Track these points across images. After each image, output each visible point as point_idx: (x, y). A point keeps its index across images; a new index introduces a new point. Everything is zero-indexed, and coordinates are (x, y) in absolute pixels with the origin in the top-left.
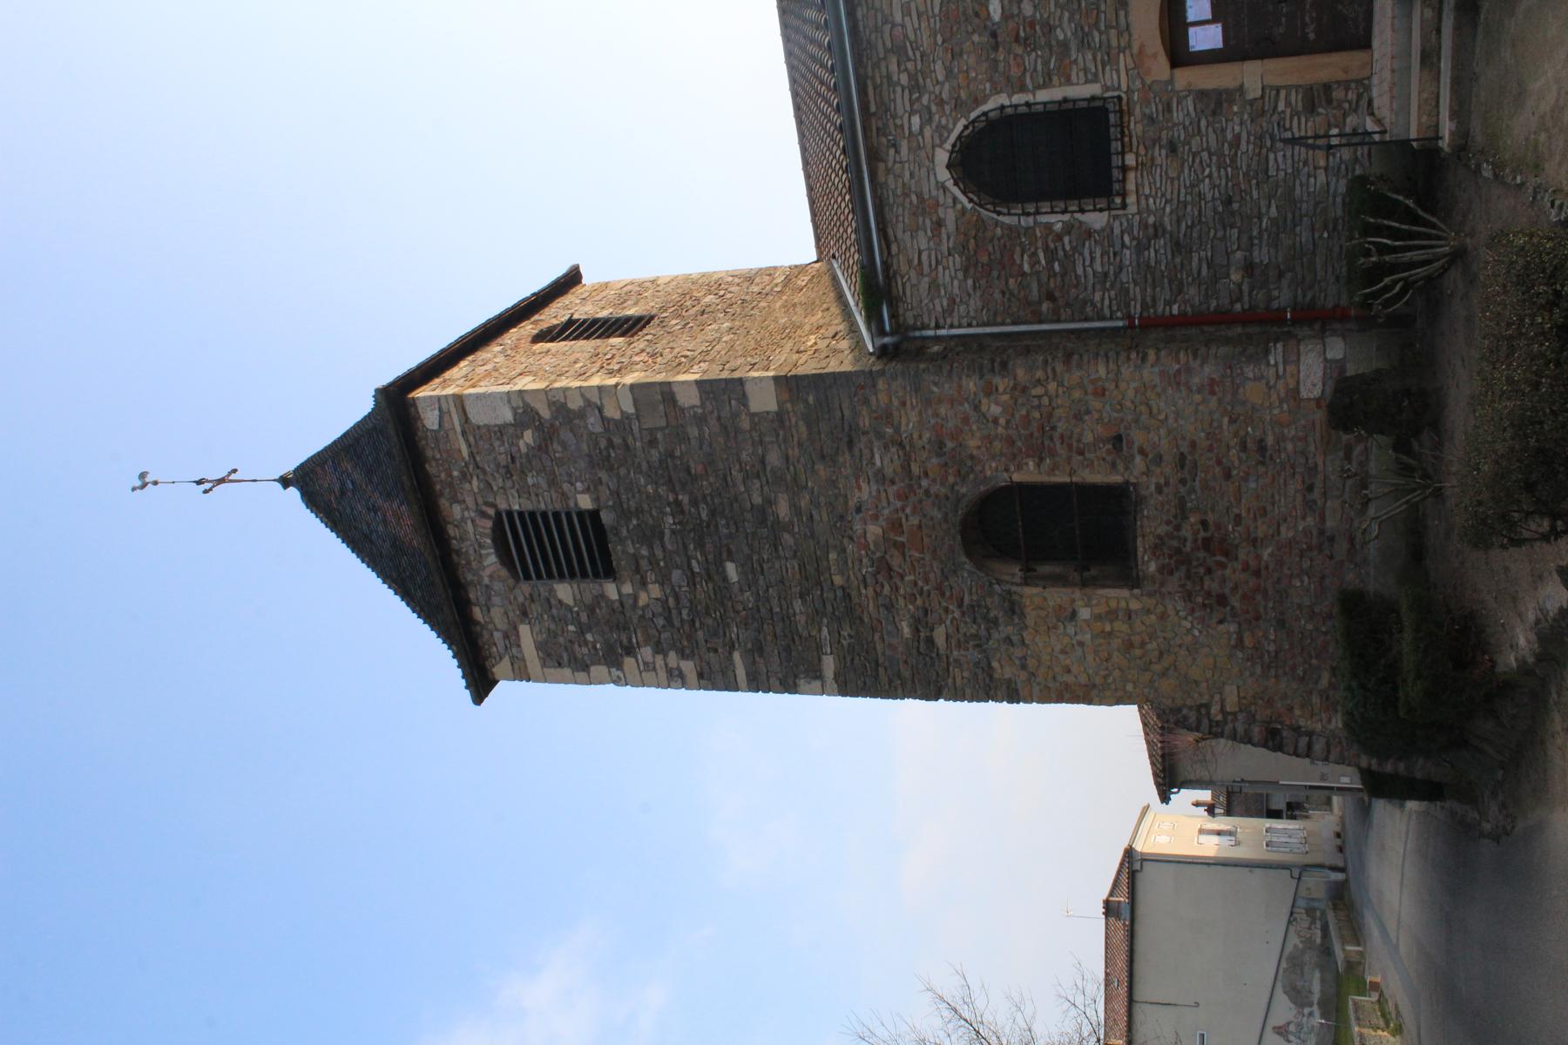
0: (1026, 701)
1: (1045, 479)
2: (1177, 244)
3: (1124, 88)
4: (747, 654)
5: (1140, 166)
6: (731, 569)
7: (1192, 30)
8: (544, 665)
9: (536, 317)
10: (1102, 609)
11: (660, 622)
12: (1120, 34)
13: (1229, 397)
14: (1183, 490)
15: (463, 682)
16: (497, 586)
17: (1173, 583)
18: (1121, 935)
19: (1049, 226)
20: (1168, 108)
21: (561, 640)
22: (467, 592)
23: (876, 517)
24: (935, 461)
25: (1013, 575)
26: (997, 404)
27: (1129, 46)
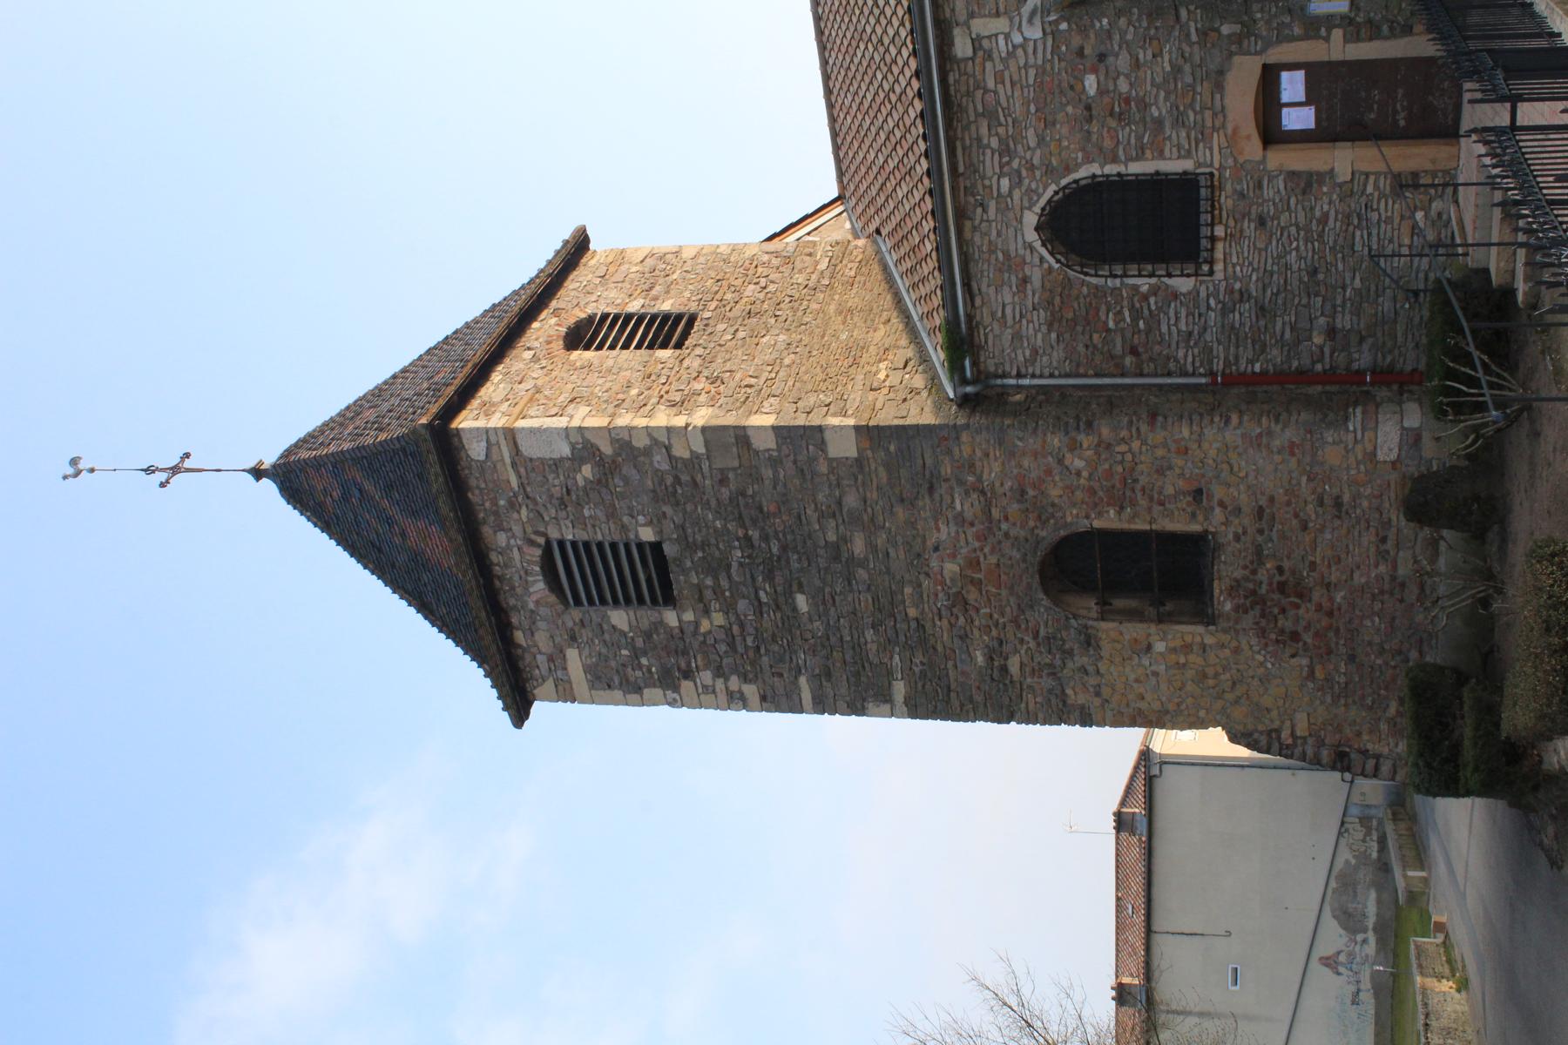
0: (1098, 725)
1: (1126, 526)
2: (1262, 308)
3: (1216, 165)
4: (813, 678)
5: (1229, 237)
6: (802, 602)
7: (1285, 110)
8: (592, 687)
9: (554, 304)
10: (1178, 643)
11: (723, 648)
12: (1215, 115)
13: (1308, 459)
14: (1260, 539)
15: (500, 704)
16: (543, 611)
17: (1248, 620)
18: (1135, 853)
19: (1135, 288)
20: (1259, 185)
21: (613, 664)
22: (508, 617)
23: (953, 556)
24: (1015, 506)
25: (1089, 609)
26: (1080, 458)
27: (1223, 126)
